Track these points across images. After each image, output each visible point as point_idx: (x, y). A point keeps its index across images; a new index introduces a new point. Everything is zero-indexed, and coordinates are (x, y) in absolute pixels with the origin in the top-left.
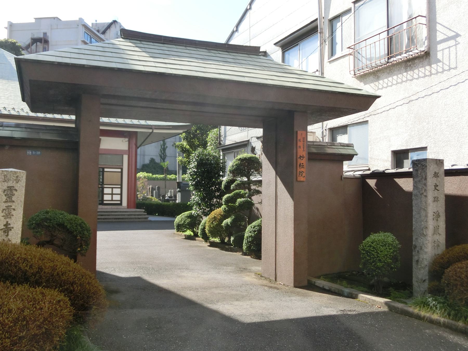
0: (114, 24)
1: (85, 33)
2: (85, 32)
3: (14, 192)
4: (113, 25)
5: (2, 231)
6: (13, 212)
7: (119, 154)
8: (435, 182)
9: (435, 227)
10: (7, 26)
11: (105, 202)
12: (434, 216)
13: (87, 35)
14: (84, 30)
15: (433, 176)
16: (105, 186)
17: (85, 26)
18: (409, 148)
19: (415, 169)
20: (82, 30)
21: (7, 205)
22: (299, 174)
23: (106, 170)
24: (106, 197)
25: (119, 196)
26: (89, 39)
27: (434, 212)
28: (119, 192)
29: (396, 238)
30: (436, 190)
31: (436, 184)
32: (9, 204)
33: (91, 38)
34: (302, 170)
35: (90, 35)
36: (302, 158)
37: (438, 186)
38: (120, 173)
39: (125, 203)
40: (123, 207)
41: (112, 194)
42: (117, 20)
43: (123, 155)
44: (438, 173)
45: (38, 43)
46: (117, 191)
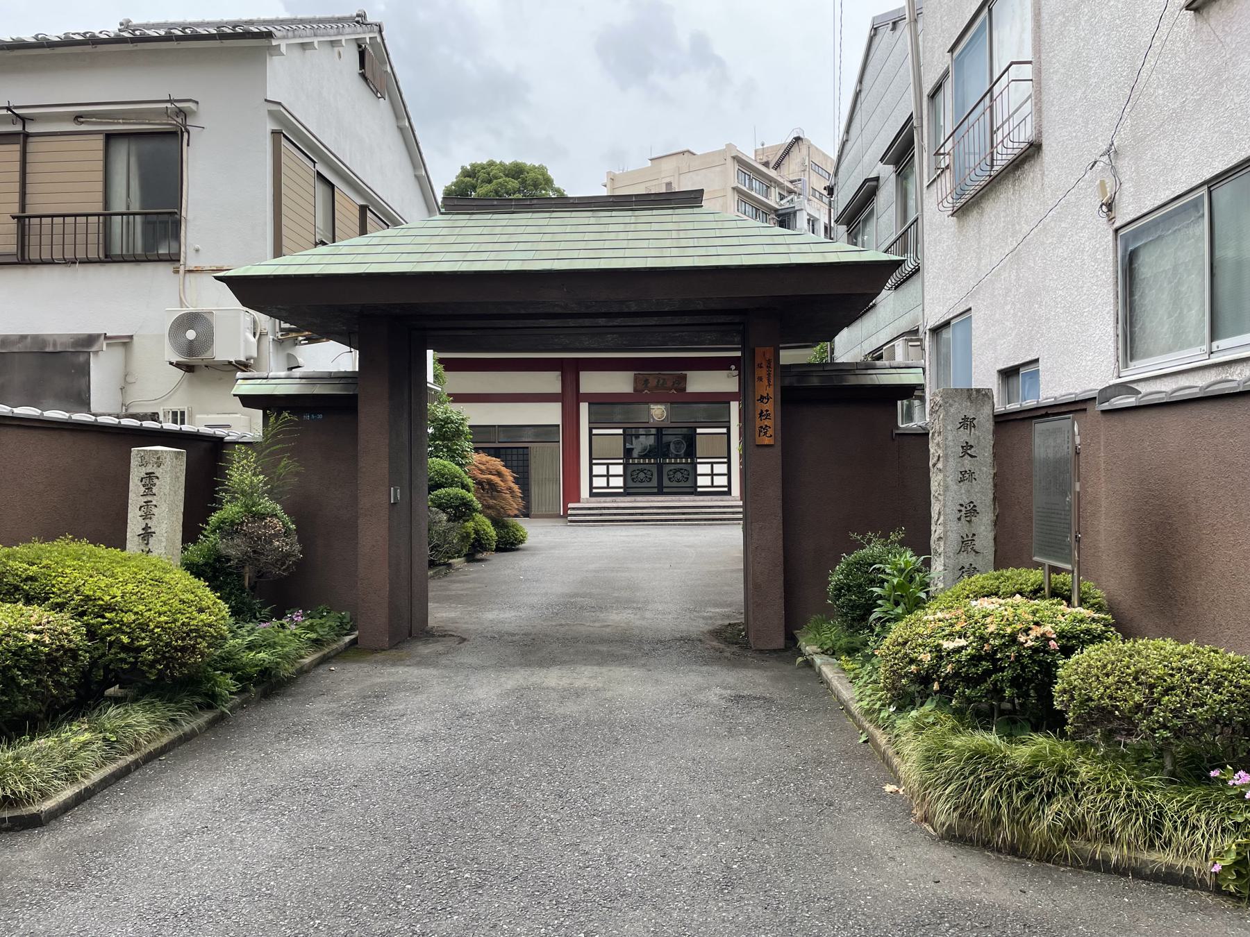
1: (740, 172)
3: (155, 481)
4: (795, 150)
5: (140, 537)
6: (155, 510)
7: (722, 400)
8: (966, 438)
9: (965, 536)
10: (605, 181)
11: (699, 490)
12: (963, 513)
14: (737, 167)
15: (959, 426)
16: (699, 460)
17: (738, 160)
18: (1017, 363)
20: (733, 168)
21: (146, 500)
22: (760, 431)
23: (699, 431)
24: (702, 481)
25: (725, 478)
27: (962, 505)
28: (725, 471)
30: (966, 456)
31: (967, 443)
32: (149, 498)
34: (767, 422)
36: (765, 401)
37: (972, 447)
41: (712, 475)
42: (802, 136)
44: (974, 419)
46: (722, 469)
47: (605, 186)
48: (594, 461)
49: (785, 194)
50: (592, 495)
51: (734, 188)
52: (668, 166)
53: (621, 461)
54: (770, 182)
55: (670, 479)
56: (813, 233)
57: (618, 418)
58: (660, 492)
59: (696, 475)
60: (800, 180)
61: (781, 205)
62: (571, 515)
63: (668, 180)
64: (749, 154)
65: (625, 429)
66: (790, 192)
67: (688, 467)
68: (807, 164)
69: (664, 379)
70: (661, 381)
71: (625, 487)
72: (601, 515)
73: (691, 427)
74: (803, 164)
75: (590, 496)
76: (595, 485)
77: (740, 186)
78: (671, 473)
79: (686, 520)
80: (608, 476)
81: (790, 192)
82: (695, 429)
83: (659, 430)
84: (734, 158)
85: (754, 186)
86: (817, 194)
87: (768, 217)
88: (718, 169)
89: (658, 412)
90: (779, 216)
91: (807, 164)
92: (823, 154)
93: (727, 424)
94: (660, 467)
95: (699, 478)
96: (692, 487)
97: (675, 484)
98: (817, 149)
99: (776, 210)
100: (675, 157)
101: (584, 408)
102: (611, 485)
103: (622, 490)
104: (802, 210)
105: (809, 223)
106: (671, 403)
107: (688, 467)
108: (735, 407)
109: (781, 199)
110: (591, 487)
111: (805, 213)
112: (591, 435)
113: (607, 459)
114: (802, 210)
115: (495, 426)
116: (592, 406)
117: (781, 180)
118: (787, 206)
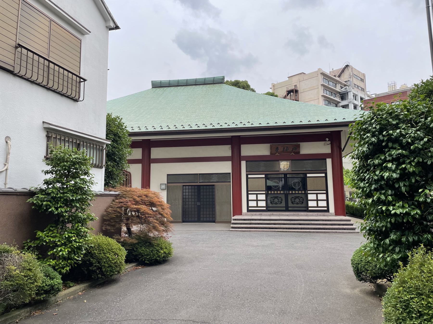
0: (347, 68)
1: (324, 79)
2: (323, 78)
4: (346, 69)
7: (322, 158)
11: (310, 209)
13: (325, 80)
14: (323, 77)
16: (309, 192)
17: (323, 74)
19: (376, 158)
20: (321, 77)
23: (308, 175)
24: (311, 204)
25: (250, 199)
26: (327, 82)
28: (325, 198)
29: (402, 151)
33: (328, 82)
35: (328, 79)
38: (325, 178)
39: (332, 209)
40: (330, 214)
42: (349, 65)
43: (326, 159)
45: (292, 93)
47: (271, 89)
48: (249, 192)
49: (343, 86)
50: (248, 211)
51: (322, 85)
52: (295, 79)
53: (264, 192)
54: (336, 82)
55: (292, 202)
56: (356, 100)
57: (262, 169)
58: (287, 209)
59: (307, 200)
60: (349, 81)
61: (342, 90)
62: (233, 224)
63: (295, 84)
64: (327, 72)
65: (266, 175)
66: (345, 85)
67: (303, 196)
68: (351, 75)
69: (287, 147)
70: (285, 148)
71: (267, 206)
72: (250, 224)
73: (304, 173)
74: (350, 75)
75: (247, 211)
76: (250, 205)
77: (324, 84)
78: (293, 199)
79: (301, 229)
80: (257, 200)
81: (345, 85)
82: (306, 174)
83: (285, 175)
84: (321, 73)
85: (330, 84)
86: (356, 86)
87: (336, 95)
88: (315, 78)
89: (284, 166)
90: (341, 95)
91: (351, 75)
92: (358, 71)
93: (325, 172)
94: (286, 196)
95: (309, 202)
96: (306, 207)
97: (275, 205)
98: (355, 69)
99: (339, 93)
100: (297, 76)
101: (243, 164)
102: (259, 205)
103: (265, 208)
104: (350, 91)
105: (353, 97)
106: (292, 160)
107: (303, 196)
108: (329, 162)
109: (342, 88)
110: (248, 207)
111: (352, 93)
112: (247, 178)
113: (257, 192)
114: (350, 91)
115: (197, 174)
116: (248, 163)
117: (341, 81)
118: (344, 90)
